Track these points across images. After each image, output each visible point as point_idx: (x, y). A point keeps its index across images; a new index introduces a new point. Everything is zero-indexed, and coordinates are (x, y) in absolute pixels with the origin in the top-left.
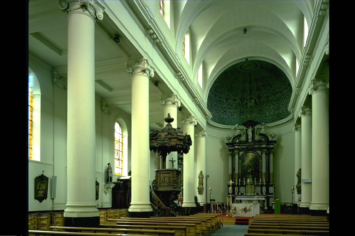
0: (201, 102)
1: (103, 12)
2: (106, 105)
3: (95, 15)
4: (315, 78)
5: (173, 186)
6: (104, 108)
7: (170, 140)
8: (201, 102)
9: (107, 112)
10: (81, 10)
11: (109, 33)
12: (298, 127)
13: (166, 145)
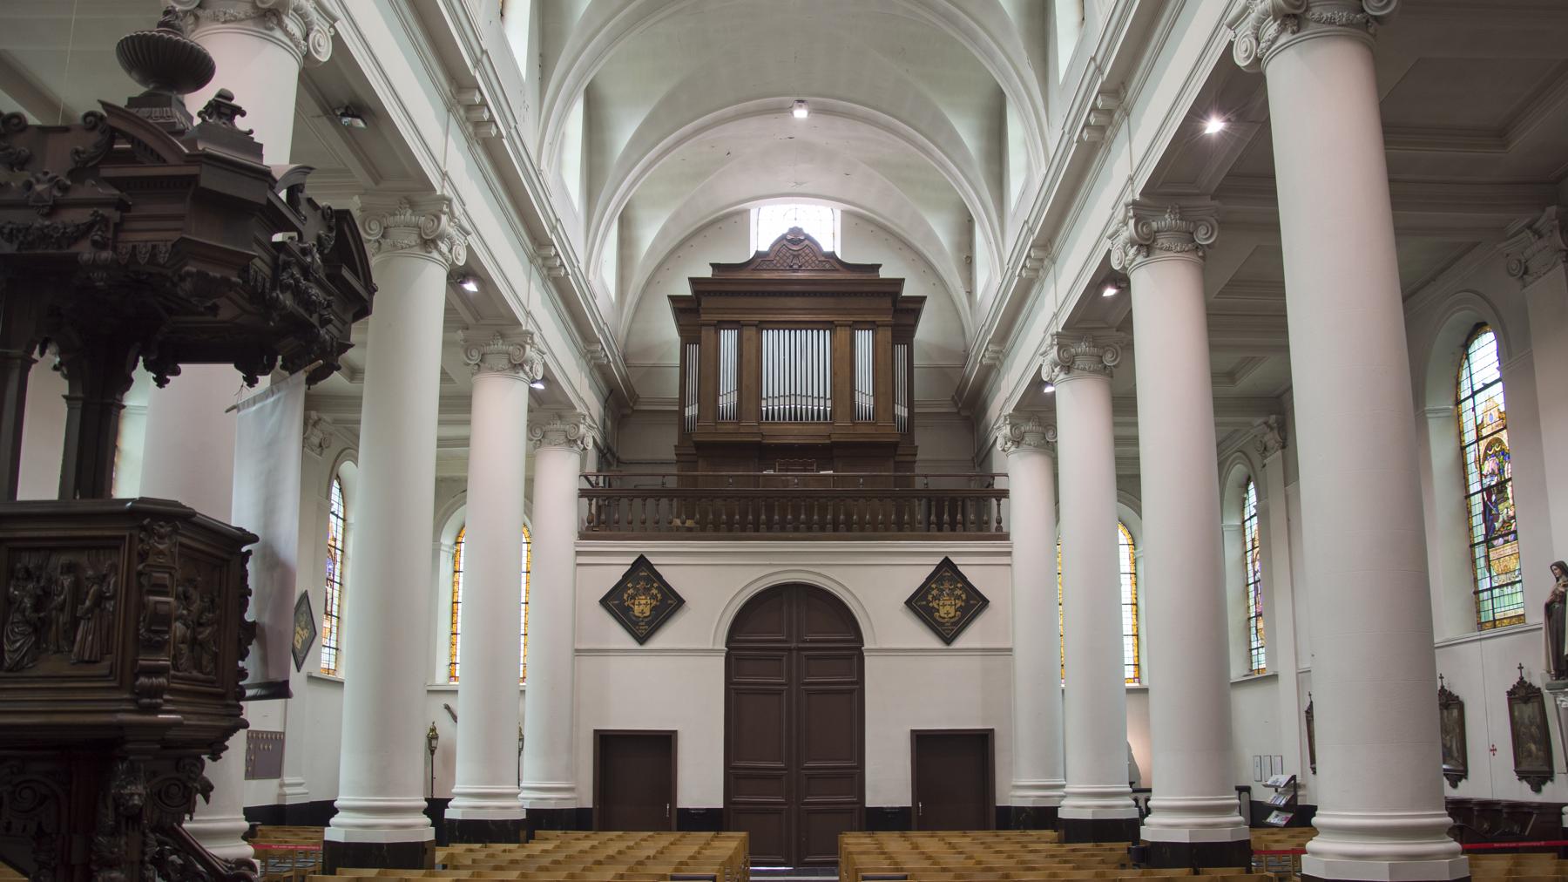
0: (509, 133)
4: (1142, 194)
5: (136, 677)
7: (122, 206)
8: (509, 133)
10: (417, 250)
12: (1154, 225)
13: (74, 249)
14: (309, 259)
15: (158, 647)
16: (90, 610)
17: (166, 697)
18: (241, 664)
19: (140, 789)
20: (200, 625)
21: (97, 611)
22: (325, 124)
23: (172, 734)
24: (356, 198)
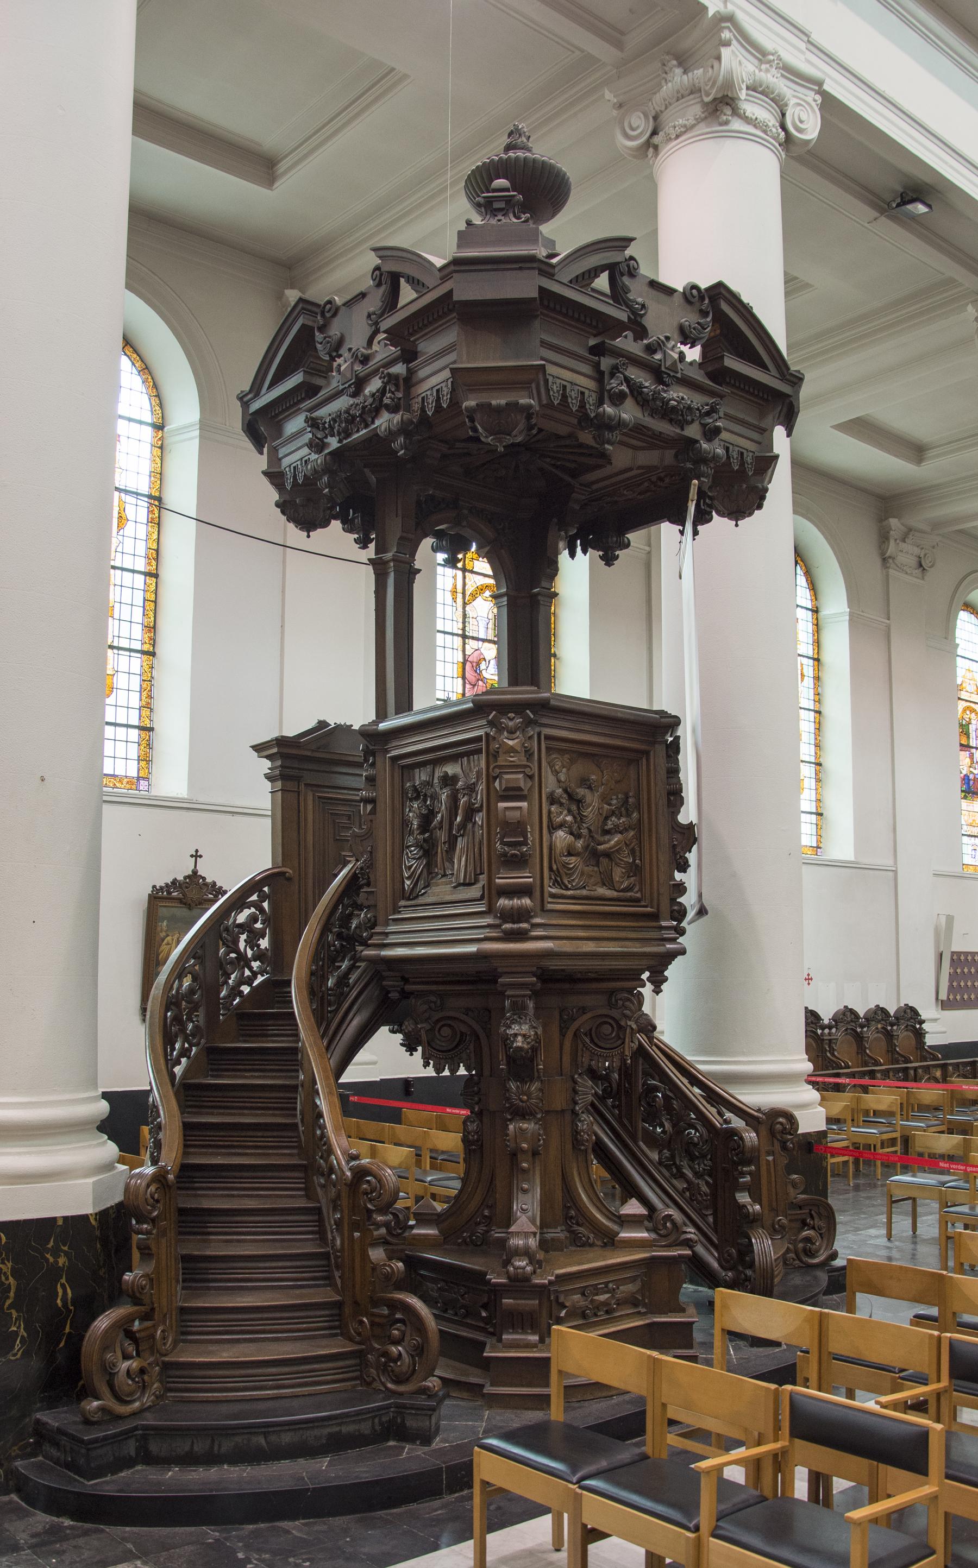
1: (819, 102)
2: (903, 528)
3: (783, 127)
6: (892, 549)
9: (913, 562)
11: (846, 176)
14: (658, 356)
15: (518, 862)
16: (463, 826)
17: (537, 920)
18: (678, 876)
19: (525, 1028)
20: (607, 832)
21: (470, 826)
22: (885, 226)
23: (554, 964)
24: (970, 308)
